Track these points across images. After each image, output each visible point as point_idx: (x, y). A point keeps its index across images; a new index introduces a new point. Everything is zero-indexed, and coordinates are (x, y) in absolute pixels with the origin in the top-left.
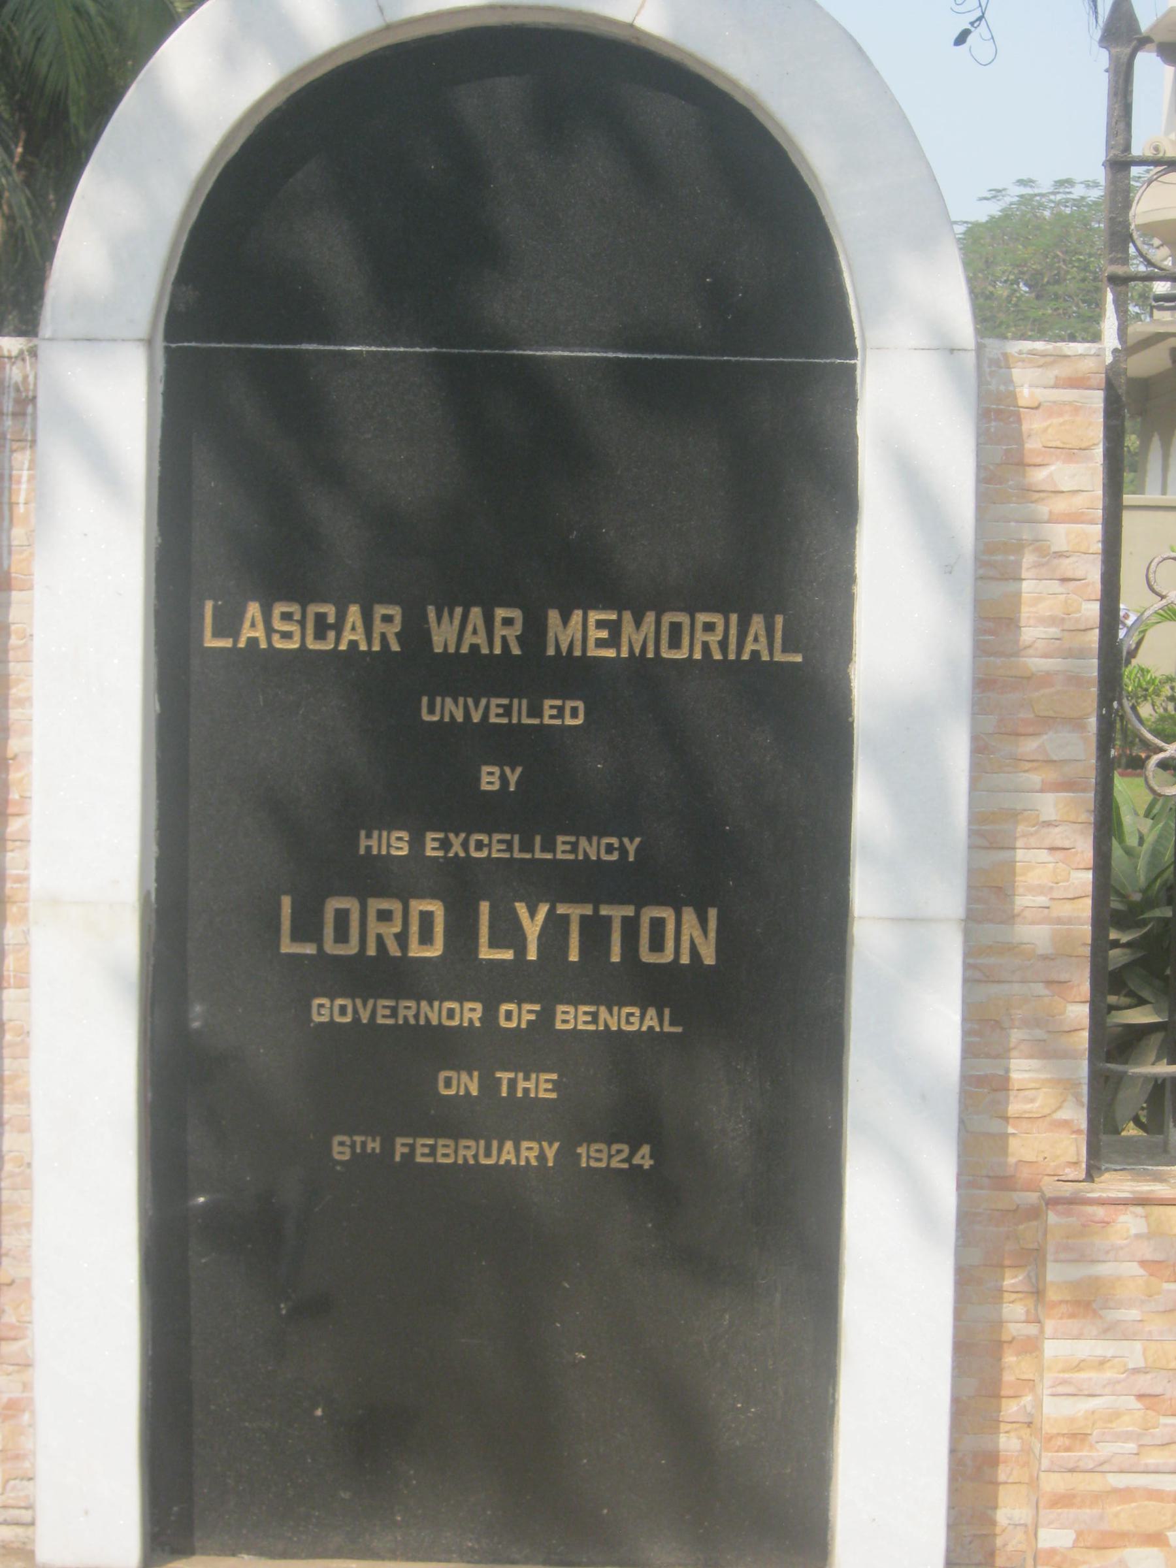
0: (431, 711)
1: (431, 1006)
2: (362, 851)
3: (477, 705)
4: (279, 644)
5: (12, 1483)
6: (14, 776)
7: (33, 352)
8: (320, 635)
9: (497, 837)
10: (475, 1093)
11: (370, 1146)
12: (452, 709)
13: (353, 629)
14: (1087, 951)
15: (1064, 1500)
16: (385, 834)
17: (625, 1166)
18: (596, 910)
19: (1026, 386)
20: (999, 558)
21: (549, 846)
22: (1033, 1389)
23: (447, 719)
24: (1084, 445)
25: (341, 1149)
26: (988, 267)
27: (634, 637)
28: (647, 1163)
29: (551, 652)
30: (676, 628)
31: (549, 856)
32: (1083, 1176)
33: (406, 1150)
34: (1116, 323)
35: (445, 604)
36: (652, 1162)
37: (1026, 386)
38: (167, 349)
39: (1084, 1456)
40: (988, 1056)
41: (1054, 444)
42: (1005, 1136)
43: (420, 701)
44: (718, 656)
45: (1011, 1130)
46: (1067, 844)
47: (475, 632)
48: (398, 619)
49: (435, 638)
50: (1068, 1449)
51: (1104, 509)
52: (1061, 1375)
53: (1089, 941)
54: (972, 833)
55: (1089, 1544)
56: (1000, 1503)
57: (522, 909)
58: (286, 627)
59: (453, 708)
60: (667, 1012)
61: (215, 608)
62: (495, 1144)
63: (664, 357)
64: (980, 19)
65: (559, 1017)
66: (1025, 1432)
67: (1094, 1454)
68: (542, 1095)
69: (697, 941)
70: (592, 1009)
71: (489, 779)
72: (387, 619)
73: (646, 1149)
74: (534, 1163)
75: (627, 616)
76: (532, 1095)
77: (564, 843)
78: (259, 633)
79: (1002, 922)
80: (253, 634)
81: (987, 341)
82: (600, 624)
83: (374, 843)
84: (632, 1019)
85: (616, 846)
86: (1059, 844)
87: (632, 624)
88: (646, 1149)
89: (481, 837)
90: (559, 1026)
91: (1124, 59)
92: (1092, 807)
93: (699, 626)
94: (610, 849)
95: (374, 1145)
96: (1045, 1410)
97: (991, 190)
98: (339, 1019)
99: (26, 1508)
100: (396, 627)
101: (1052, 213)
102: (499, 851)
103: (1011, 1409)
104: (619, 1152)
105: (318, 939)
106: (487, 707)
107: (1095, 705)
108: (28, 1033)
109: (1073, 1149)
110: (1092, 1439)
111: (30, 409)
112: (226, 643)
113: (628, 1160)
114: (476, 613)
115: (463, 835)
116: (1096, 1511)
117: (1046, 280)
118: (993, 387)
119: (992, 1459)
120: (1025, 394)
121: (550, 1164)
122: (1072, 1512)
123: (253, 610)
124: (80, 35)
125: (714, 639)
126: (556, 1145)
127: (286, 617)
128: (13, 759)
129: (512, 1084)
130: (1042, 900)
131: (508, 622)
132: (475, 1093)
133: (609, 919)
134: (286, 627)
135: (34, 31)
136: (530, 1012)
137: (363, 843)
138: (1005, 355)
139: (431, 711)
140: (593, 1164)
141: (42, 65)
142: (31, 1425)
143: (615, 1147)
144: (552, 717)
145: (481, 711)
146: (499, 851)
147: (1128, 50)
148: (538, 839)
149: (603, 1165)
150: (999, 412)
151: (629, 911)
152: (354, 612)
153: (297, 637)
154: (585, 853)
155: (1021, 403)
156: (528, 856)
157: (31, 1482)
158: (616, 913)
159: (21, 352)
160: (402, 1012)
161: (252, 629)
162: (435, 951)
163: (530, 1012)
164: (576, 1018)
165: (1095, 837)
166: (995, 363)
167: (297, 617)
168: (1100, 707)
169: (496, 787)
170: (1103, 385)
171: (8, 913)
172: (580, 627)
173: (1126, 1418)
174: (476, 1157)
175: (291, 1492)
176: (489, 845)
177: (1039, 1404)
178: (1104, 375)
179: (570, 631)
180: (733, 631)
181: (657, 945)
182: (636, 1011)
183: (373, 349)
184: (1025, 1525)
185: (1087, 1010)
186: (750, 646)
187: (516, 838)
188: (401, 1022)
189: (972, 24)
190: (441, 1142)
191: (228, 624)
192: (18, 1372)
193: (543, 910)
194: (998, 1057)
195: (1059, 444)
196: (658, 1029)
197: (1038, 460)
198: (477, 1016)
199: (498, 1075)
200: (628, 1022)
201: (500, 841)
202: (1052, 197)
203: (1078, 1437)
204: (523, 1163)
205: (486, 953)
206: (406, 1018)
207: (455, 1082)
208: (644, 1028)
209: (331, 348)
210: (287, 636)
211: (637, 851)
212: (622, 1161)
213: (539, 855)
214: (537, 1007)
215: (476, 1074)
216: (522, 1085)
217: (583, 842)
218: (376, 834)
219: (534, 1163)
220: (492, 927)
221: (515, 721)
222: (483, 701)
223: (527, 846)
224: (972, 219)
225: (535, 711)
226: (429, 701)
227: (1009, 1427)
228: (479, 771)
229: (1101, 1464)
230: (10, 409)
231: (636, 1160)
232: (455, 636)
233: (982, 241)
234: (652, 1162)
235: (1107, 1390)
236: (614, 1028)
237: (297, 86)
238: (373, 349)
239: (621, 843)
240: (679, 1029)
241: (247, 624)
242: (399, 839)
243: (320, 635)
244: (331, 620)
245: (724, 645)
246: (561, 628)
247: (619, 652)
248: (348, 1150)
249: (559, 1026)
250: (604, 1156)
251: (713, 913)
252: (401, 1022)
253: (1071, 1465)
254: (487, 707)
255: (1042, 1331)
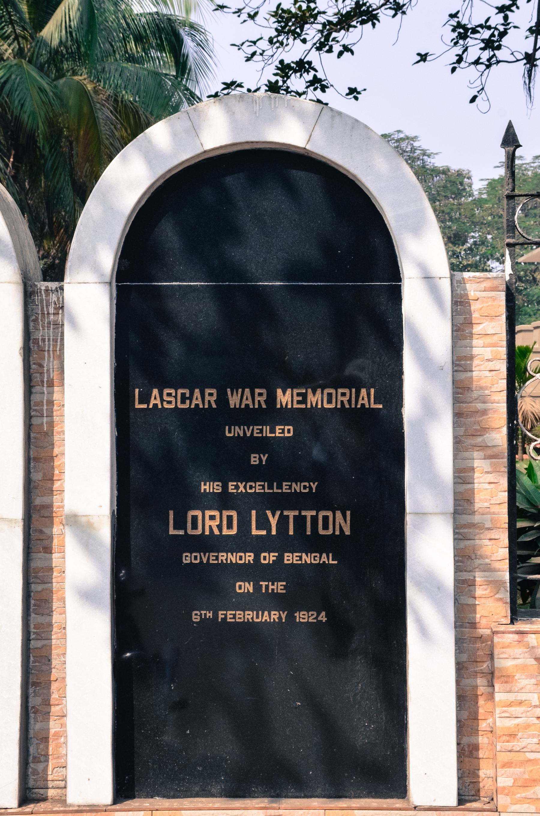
0: (230, 432)
1: (233, 555)
2: (202, 491)
3: (248, 429)
4: (166, 406)
5: (56, 769)
6: (56, 463)
7: (62, 288)
8: (183, 402)
9: (258, 484)
10: (251, 591)
11: (208, 615)
12: (238, 431)
13: (197, 399)
14: (507, 526)
15: (507, 765)
16: (212, 483)
17: (315, 621)
18: (300, 513)
19: (472, 291)
20: (463, 362)
21: (280, 487)
22: (492, 716)
23: (236, 435)
24: (497, 315)
25: (196, 617)
26: (500, 202)
27: (313, 399)
28: (324, 619)
29: (279, 406)
30: (330, 395)
31: (280, 491)
32: (509, 622)
33: (223, 616)
34: (510, 263)
35: (234, 388)
36: (326, 619)
37: (472, 291)
38: (117, 286)
39: (516, 745)
40: (466, 571)
41: (485, 315)
42: (475, 605)
43: (225, 428)
44: (347, 406)
45: (477, 603)
46: (496, 481)
47: (247, 399)
48: (215, 395)
49: (230, 402)
50: (508, 742)
51: (507, 341)
52: (503, 709)
53: (507, 521)
54: (455, 477)
55: (520, 785)
56: (481, 768)
57: (269, 513)
58: (169, 399)
59: (239, 431)
60: (331, 555)
61: (139, 392)
62: (260, 613)
63: (322, 284)
64: (483, 89)
65: (286, 558)
66: (490, 735)
67: (519, 744)
68: (279, 591)
69: (342, 525)
70: (299, 554)
71: (254, 460)
72: (211, 394)
73: (323, 614)
74: (277, 620)
75: (310, 391)
76: (275, 592)
77: (286, 485)
78: (158, 402)
79: (470, 514)
80: (155, 402)
81: (455, 273)
82: (298, 394)
83: (207, 487)
84: (316, 558)
85: (308, 486)
86: (492, 481)
87: (312, 394)
88: (323, 614)
89: (252, 484)
90: (286, 562)
91: (511, 153)
92: (506, 465)
93: (339, 394)
94: (305, 487)
95: (210, 615)
96: (497, 724)
97: (500, 162)
98: (194, 562)
99: (62, 781)
100: (215, 397)
101: (532, 173)
102: (259, 489)
103: (483, 725)
104: (312, 615)
105: (185, 528)
106: (253, 430)
107: (506, 423)
108: (64, 572)
109: (504, 611)
110: (518, 737)
111: (60, 312)
112: (145, 406)
113: (316, 618)
114: (247, 391)
115: (244, 483)
116: (522, 770)
117: (530, 207)
118: (458, 292)
119: (476, 747)
120: (472, 294)
121: (284, 621)
122: (512, 770)
123: (155, 392)
124: (43, 102)
125: (345, 399)
126: (286, 613)
127: (169, 395)
128: (56, 457)
129: (267, 587)
130: (486, 504)
131: (260, 394)
132: (251, 591)
133: (305, 517)
134: (169, 399)
135: (19, 101)
136: (273, 556)
137: (203, 487)
138: (463, 278)
139: (230, 432)
140: (302, 620)
141: (25, 117)
142: (66, 743)
143: (310, 613)
144: (279, 433)
145: (250, 431)
146: (259, 489)
147: (512, 149)
148: (275, 484)
149: (306, 620)
150: (460, 302)
151: (314, 513)
152: (197, 392)
153: (174, 403)
154: (295, 489)
155: (470, 298)
156: (271, 491)
157: (65, 768)
158: (309, 514)
159: (57, 288)
160: (220, 558)
161: (155, 400)
162: (234, 531)
163: (273, 556)
164: (293, 558)
165: (508, 478)
166: (459, 282)
167: (174, 394)
168: (508, 423)
169: (257, 463)
170: (505, 289)
171: (54, 521)
172: (290, 396)
173: (533, 728)
174: (252, 618)
175: (177, 768)
176: (255, 487)
177: (495, 723)
178: (505, 286)
179: (286, 397)
180: (353, 396)
181: (326, 527)
182: (318, 555)
183: (202, 283)
184: (493, 778)
185: (508, 551)
186: (360, 402)
187: (266, 484)
188: (220, 562)
189: (478, 92)
190: (238, 612)
191: (145, 398)
192: (59, 719)
193: (278, 513)
194: (470, 571)
195: (486, 314)
196: (327, 562)
197: (478, 322)
198: (251, 559)
199: (261, 583)
200: (314, 560)
201: (259, 485)
202: (532, 165)
203: (512, 736)
204: (272, 621)
205: (255, 532)
206: (222, 560)
207: (243, 587)
208: (321, 562)
209: (185, 284)
210: (169, 402)
211: (316, 488)
212: (313, 619)
213: (275, 490)
214: (276, 554)
215: (252, 583)
216: (271, 587)
217: (294, 485)
218: (208, 484)
219: (277, 620)
220: (257, 521)
221: (264, 435)
222: (251, 427)
223: (271, 487)
224: (491, 177)
225: (273, 431)
226: (229, 428)
227: (483, 733)
228: (250, 456)
229: (523, 748)
230: (52, 312)
231: (320, 618)
232: (239, 401)
233: (496, 189)
234: (326, 619)
235: (524, 715)
236: (309, 562)
237: (168, 177)
238: (202, 283)
239: (310, 485)
240: (336, 562)
241: (153, 398)
242: (218, 485)
243: (183, 402)
244: (188, 395)
245: (350, 401)
246: (282, 396)
247: (306, 406)
248: (199, 617)
249: (286, 562)
250: (306, 617)
251: (348, 513)
252: (220, 562)
253: (509, 749)
254: (253, 430)
255: (494, 690)
